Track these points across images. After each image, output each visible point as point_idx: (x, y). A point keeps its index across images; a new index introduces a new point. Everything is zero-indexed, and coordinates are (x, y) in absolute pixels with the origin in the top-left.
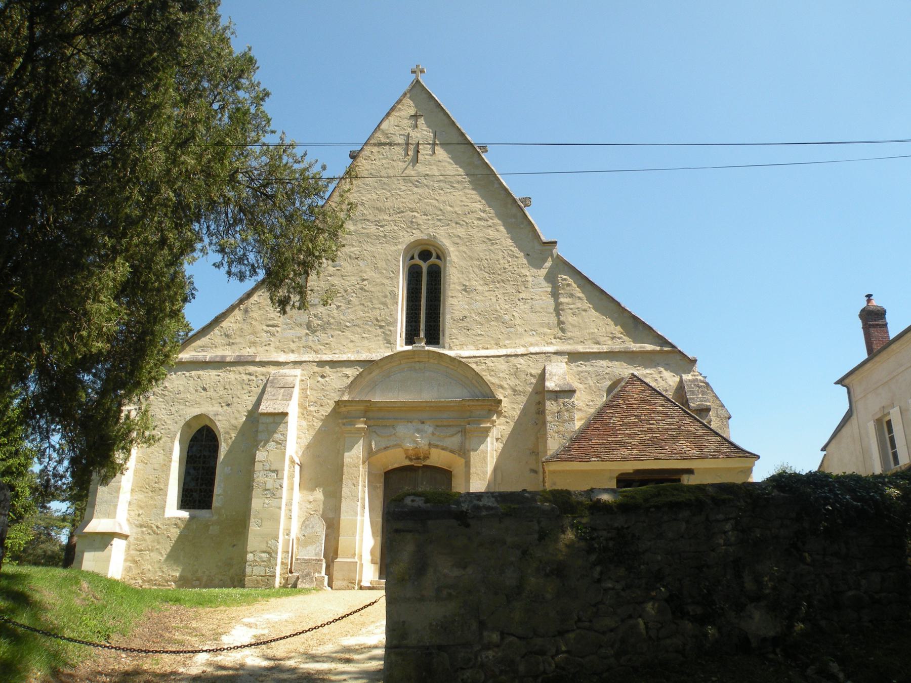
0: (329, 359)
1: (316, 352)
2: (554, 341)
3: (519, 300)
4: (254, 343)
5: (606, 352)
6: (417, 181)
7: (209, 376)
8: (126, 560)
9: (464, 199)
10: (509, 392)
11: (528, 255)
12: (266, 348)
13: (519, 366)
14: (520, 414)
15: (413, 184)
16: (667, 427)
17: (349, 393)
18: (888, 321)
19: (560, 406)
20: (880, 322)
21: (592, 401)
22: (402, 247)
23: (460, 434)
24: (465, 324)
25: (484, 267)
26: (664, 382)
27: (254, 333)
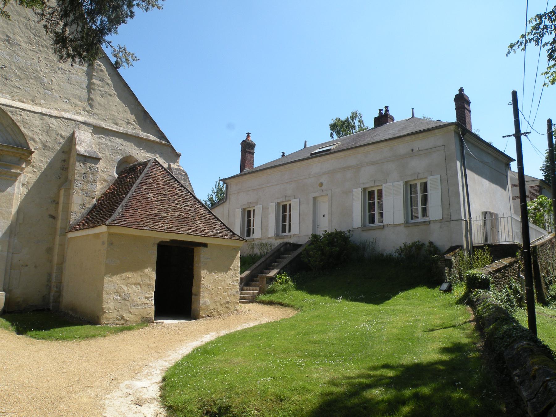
2: (82, 112)
3: (59, 69)
5: (122, 133)
10: (39, 146)
13: (51, 126)
14: (47, 166)
16: (187, 208)
18: (255, 151)
19: (87, 168)
20: (251, 151)
21: (106, 168)
25: (31, 28)
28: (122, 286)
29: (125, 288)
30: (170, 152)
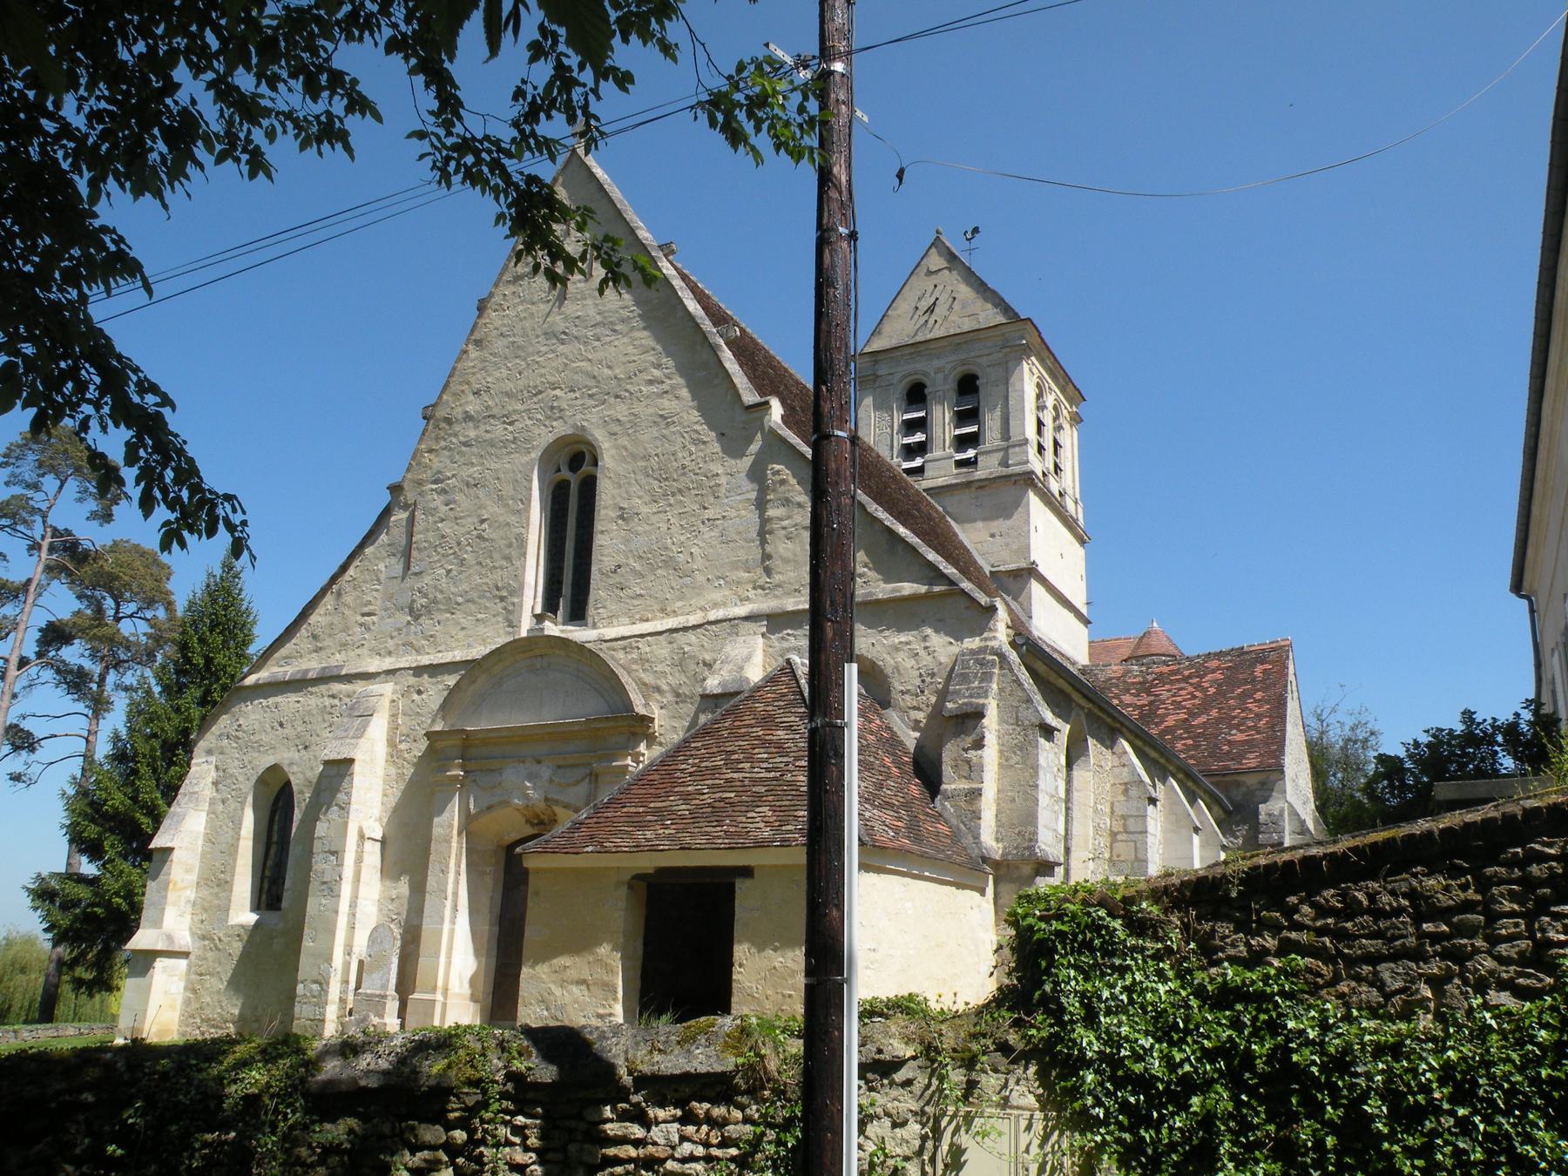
0: (427, 663)
1: (418, 651)
2: (751, 594)
3: (703, 523)
4: (345, 645)
6: (564, 333)
7: (288, 701)
8: (186, 989)
9: (630, 349)
10: (670, 697)
11: (723, 434)
12: (358, 651)
15: (558, 339)
17: (444, 718)
22: (535, 455)
23: (587, 781)
24: (618, 580)
26: (929, 658)
27: (346, 629)
28: (553, 987)
29: (558, 992)
30: (967, 608)
